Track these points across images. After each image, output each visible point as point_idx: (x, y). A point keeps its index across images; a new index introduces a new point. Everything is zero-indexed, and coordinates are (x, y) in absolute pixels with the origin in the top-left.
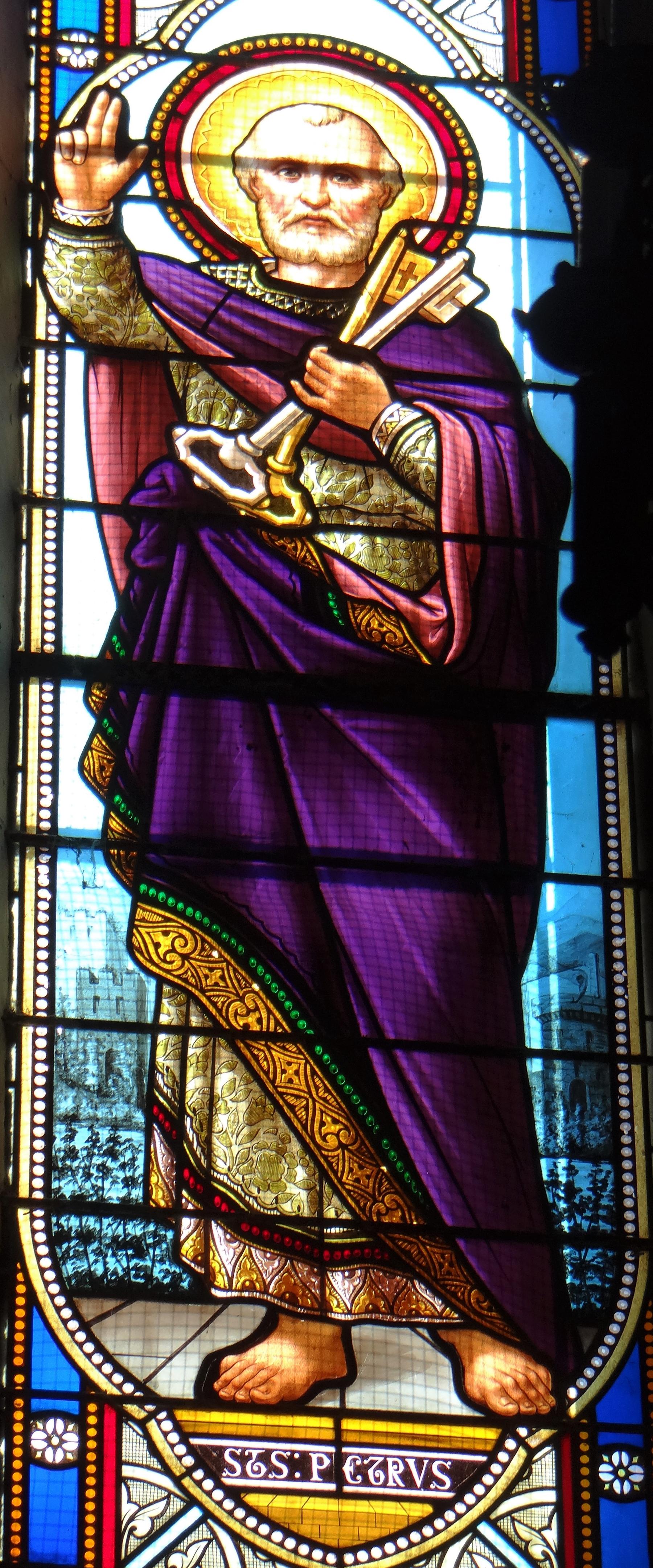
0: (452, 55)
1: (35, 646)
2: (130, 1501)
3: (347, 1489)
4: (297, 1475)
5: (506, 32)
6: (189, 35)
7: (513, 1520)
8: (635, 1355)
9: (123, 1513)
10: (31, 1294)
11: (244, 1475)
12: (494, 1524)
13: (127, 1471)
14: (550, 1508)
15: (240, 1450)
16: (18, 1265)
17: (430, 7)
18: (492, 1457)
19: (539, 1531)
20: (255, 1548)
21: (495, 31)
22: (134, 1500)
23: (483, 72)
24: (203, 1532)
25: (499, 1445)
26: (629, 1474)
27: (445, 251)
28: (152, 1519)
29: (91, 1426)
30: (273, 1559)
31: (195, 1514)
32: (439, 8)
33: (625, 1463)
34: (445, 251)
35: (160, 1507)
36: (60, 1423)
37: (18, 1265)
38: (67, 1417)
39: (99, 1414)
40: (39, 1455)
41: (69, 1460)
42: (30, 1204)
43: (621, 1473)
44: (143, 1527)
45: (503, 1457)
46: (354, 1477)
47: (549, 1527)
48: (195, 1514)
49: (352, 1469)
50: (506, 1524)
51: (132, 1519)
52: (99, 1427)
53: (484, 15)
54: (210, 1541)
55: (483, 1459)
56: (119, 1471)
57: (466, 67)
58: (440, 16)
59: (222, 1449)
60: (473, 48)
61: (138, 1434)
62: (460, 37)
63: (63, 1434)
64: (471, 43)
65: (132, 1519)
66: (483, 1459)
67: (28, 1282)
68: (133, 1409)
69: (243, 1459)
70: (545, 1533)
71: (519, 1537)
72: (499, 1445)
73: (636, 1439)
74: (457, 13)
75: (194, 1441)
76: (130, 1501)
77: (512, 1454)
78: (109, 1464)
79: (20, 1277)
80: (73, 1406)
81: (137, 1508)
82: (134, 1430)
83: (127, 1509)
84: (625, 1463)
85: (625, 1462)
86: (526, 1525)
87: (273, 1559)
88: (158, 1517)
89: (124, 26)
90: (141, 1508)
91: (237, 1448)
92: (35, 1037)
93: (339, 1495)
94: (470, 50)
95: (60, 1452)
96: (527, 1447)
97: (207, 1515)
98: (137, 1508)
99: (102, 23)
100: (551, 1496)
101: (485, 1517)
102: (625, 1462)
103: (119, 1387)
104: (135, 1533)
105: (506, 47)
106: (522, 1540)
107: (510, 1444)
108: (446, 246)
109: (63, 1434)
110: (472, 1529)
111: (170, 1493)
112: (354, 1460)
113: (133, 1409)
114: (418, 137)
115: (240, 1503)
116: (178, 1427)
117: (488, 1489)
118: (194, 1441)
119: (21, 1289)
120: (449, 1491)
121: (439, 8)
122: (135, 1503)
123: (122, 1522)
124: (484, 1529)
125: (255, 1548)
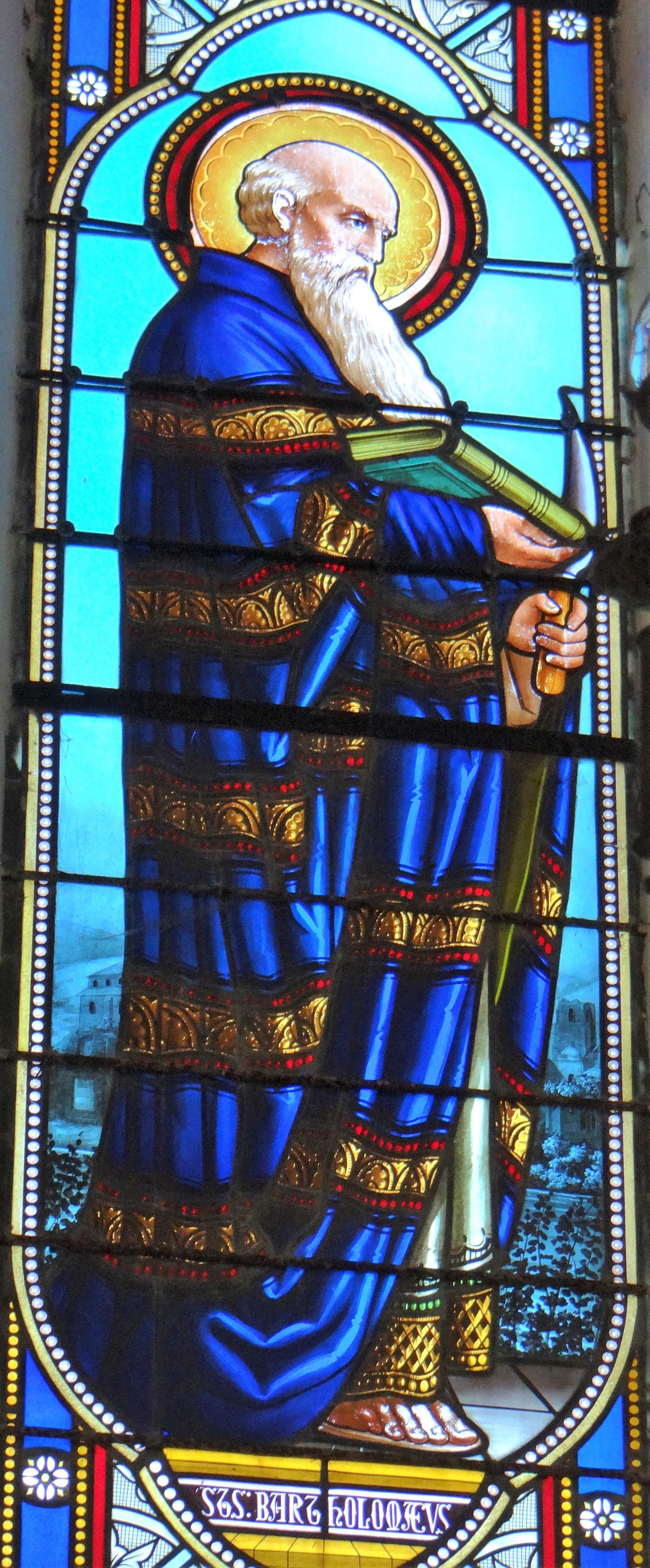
0: (461, 89)
1: (35, 676)
2: (118, 1544)
3: (332, 1531)
5: (514, 71)
6: (199, 71)
7: (184, 24)
9: (113, 1556)
10: (23, 1334)
12: (201, 20)
13: (116, 1514)
14: (530, 1550)
16: (11, 1305)
17: (197, 1559)
18: (476, 1505)
19: (162, 13)
20: (401, 15)
21: (506, 68)
22: (122, 1544)
24: (445, 30)
25: (482, 1491)
26: (610, 1522)
28: (486, 40)
30: (388, 8)
31: (451, 44)
32: (184, 1556)
33: (607, 1511)
35: (147, 1551)
36: (41, 1495)
37: (11, 1305)
38: (57, 1455)
39: (90, 1456)
40: (30, 1492)
41: (59, 1497)
42: (24, 1242)
43: (603, 1521)
44: (494, 36)
45: (486, 1502)
47: (153, 17)
48: (451, 44)
50: (191, 21)
51: (504, 42)
52: (89, 1469)
53: (130, 1548)
54: (439, 23)
55: (467, 1501)
56: (108, 1513)
57: (475, 102)
58: (184, 1545)
60: (484, 86)
61: (501, 104)
62: (160, 1517)
63: (54, 1471)
64: (147, 1508)
65: (504, 42)
66: (467, 1501)
67: (20, 1321)
68: (123, 1448)
70: (157, 13)
71: (180, 12)
72: (482, 1491)
73: (617, 1486)
74: (163, 1550)
75: (182, 1481)
76: (118, 1544)
78: (99, 1509)
79: (13, 1316)
80: (63, 1445)
81: (124, 1552)
82: (123, 1475)
83: (508, 49)
84: (607, 1511)
85: (607, 1510)
86: (172, 19)
87: (388, 8)
88: (482, 42)
89: (549, 1510)
90: (129, 1552)
92: (25, 1259)
93: (324, 1535)
94: (149, 1500)
95: (51, 1488)
97: (442, 42)
98: (124, 1552)
99: (112, 57)
100: (533, 1538)
101: (208, 27)
102: (607, 1510)
103: (110, 1427)
104: (501, 33)
105: (515, 84)
106: (178, 9)
108: (49, 174)
109: (54, 1471)
110: (219, 19)
111: (159, 1537)
113: (123, 1448)
115: (228, 1546)
116: (167, 1469)
117: (471, 1534)
118: (182, 1481)
119: (14, 1328)
120: (317, 1525)
121: (184, 1556)
122: (123, 1547)
123: (111, 1563)
124: (209, 18)
125: (401, 15)
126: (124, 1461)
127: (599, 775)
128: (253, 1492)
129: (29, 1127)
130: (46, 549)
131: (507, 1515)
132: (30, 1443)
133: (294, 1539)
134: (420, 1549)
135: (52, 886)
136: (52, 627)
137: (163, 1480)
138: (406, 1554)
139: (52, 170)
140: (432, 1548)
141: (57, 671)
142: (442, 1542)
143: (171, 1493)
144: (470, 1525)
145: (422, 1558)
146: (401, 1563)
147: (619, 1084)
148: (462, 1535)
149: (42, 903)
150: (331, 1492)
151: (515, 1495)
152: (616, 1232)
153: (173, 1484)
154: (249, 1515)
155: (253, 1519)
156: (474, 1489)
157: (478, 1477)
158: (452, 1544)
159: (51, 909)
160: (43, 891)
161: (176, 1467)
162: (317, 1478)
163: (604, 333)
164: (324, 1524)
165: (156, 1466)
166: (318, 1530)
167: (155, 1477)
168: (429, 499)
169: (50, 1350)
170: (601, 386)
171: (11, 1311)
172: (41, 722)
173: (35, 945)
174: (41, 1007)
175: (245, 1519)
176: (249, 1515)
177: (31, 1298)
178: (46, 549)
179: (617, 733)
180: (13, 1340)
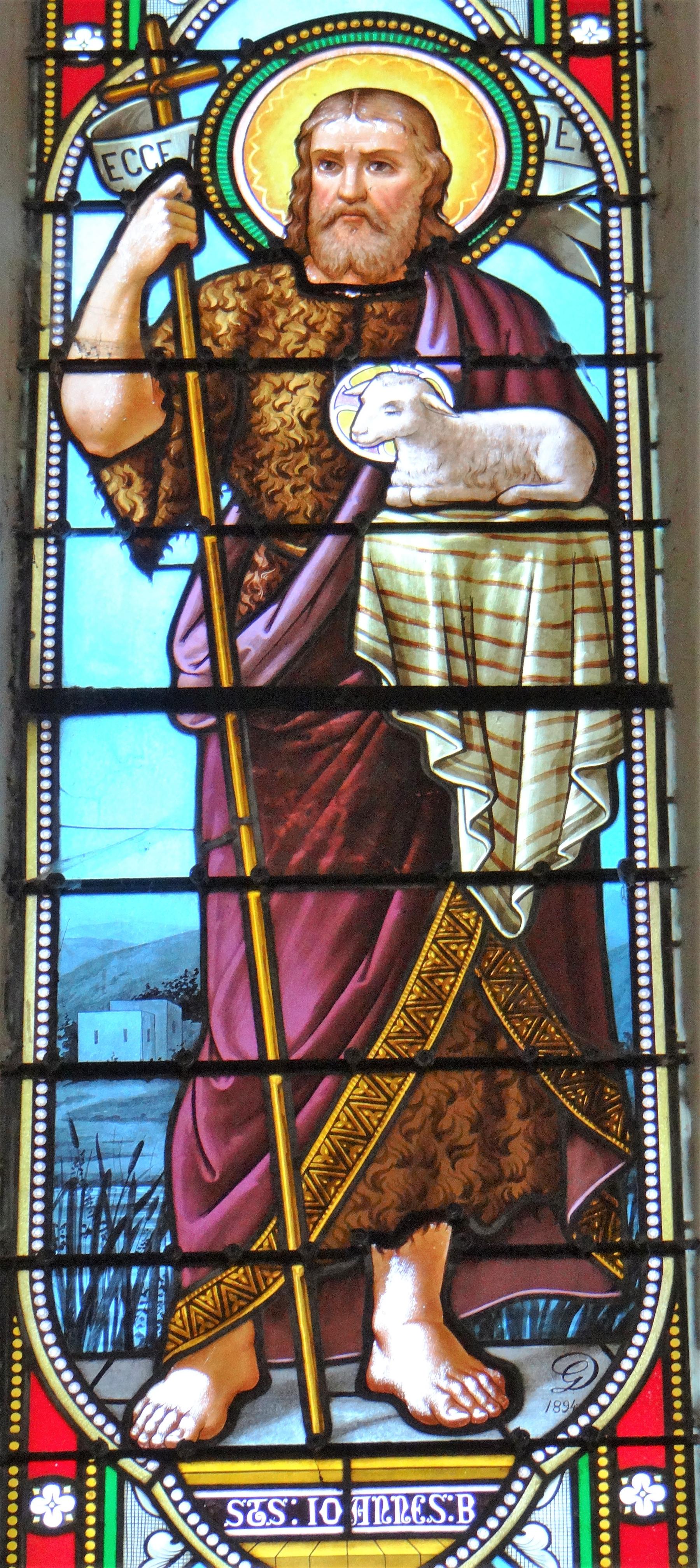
3: (355, 1530)
4: (294, 1522)
8: (657, 1374)
10: (28, 1350)
11: (245, 1525)
15: (286, 1500)
18: (506, 1488)
23: (509, 32)
25: (513, 1474)
27: (46, 159)
29: (602, 1480)
34: (46, 159)
37: (15, 1320)
40: (628, 1510)
45: (517, 1486)
46: (419, 1519)
49: (419, 1509)
55: (494, 1488)
59: (225, 1501)
66: (494, 1488)
67: (25, 1336)
69: (245, 1510)
72: (513, 1474)
75: (200, 1495)
77: (526, 1482)
79: (16, 1331)
91: (282, 1498)
92: (32, 1281)
93: (348, 1536)
96: (541, 1473)
107: (524, 1472)
108: (45, 154)
112: (419, 1499)
114: (461, 93)
116: (181, 1483)
118: (200, 1495)
120: (338, 1524)
126: (136, 1482)
127: (632, 900)
128: (453, 1494)
129: (33, 1200)
130: (35, 1085)
131: (539, 1494)
132: (626, 1454)
133: (315, 1544)
134: (447, 1543)
135: (60, 545)
136: (49, 935)
137: (177, 1494)
138: (433, 1548)
139: (49, 141)
140: (460, 1540)
141: (58, 672)
142: (472, 1532)
143: (185, 1507)
144: (501, 1511)
145: (451, 1552)
146: (428, 1559)
147: (652, 1037)
148: (492, 1523)
149: (45, 917)
150: (354, 1492)
151: (546, 1479)
152: (651, 1194)
153: (188, 1496)
154: (451, 1519)
155: (454, 1523)
156: (503, 1475)
157: (507, 1461)
158: (483, 1533)
159: (55, 923)
160: (52, 550)
161: (191, 1480)
162: (338, 1477)
163: (625, 260)
164: (346, 1520)
165: (170, 1481)
166: (340, 1530)
167: (168, 1491)
168: (448, 661)
169: (59, 1373)
170: (629, 489)
171: (15, 1325)
172: (40, 730)
173: (35, 1134)
174: (47, 960)
175: (447, 1523)
176: (451, 1519)
177: (38, 1321)
178: (35, 1085)
179: (644, 678)
180: (17, 1355)
